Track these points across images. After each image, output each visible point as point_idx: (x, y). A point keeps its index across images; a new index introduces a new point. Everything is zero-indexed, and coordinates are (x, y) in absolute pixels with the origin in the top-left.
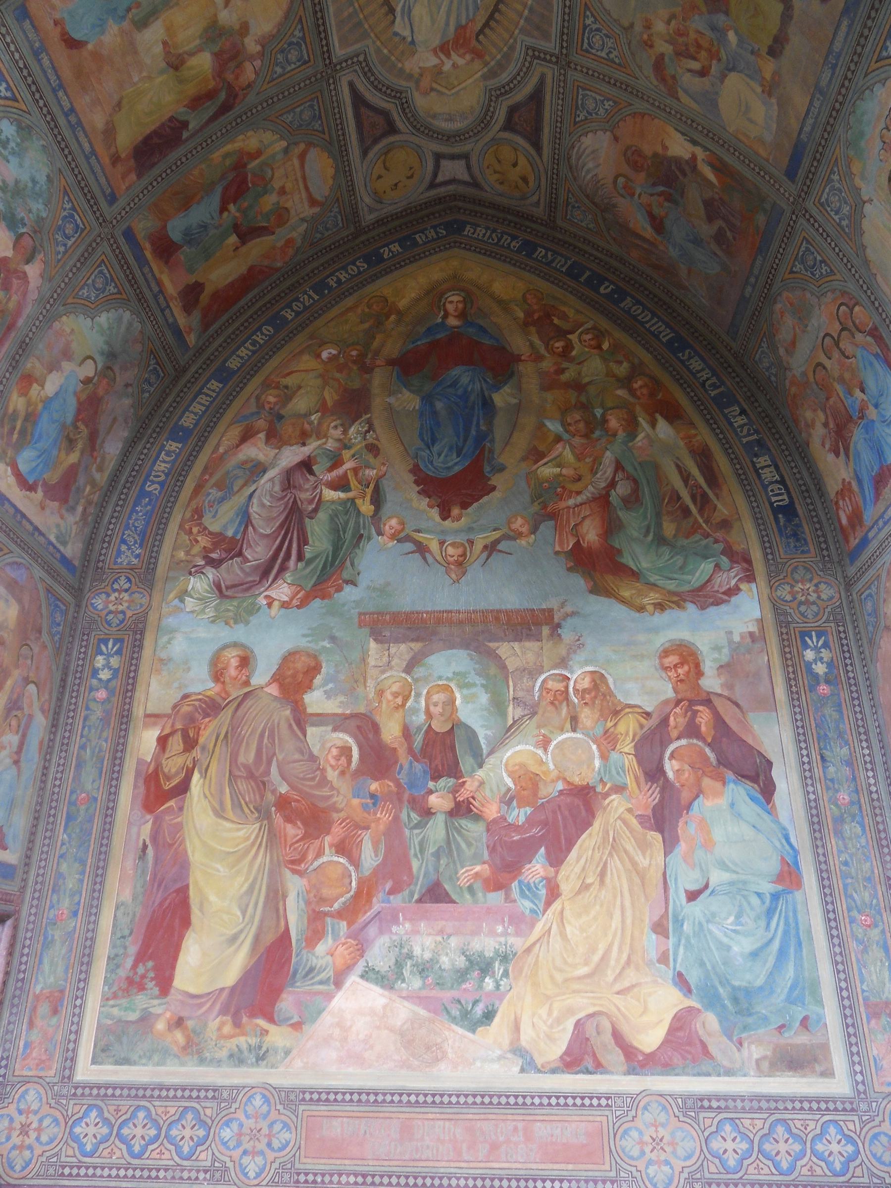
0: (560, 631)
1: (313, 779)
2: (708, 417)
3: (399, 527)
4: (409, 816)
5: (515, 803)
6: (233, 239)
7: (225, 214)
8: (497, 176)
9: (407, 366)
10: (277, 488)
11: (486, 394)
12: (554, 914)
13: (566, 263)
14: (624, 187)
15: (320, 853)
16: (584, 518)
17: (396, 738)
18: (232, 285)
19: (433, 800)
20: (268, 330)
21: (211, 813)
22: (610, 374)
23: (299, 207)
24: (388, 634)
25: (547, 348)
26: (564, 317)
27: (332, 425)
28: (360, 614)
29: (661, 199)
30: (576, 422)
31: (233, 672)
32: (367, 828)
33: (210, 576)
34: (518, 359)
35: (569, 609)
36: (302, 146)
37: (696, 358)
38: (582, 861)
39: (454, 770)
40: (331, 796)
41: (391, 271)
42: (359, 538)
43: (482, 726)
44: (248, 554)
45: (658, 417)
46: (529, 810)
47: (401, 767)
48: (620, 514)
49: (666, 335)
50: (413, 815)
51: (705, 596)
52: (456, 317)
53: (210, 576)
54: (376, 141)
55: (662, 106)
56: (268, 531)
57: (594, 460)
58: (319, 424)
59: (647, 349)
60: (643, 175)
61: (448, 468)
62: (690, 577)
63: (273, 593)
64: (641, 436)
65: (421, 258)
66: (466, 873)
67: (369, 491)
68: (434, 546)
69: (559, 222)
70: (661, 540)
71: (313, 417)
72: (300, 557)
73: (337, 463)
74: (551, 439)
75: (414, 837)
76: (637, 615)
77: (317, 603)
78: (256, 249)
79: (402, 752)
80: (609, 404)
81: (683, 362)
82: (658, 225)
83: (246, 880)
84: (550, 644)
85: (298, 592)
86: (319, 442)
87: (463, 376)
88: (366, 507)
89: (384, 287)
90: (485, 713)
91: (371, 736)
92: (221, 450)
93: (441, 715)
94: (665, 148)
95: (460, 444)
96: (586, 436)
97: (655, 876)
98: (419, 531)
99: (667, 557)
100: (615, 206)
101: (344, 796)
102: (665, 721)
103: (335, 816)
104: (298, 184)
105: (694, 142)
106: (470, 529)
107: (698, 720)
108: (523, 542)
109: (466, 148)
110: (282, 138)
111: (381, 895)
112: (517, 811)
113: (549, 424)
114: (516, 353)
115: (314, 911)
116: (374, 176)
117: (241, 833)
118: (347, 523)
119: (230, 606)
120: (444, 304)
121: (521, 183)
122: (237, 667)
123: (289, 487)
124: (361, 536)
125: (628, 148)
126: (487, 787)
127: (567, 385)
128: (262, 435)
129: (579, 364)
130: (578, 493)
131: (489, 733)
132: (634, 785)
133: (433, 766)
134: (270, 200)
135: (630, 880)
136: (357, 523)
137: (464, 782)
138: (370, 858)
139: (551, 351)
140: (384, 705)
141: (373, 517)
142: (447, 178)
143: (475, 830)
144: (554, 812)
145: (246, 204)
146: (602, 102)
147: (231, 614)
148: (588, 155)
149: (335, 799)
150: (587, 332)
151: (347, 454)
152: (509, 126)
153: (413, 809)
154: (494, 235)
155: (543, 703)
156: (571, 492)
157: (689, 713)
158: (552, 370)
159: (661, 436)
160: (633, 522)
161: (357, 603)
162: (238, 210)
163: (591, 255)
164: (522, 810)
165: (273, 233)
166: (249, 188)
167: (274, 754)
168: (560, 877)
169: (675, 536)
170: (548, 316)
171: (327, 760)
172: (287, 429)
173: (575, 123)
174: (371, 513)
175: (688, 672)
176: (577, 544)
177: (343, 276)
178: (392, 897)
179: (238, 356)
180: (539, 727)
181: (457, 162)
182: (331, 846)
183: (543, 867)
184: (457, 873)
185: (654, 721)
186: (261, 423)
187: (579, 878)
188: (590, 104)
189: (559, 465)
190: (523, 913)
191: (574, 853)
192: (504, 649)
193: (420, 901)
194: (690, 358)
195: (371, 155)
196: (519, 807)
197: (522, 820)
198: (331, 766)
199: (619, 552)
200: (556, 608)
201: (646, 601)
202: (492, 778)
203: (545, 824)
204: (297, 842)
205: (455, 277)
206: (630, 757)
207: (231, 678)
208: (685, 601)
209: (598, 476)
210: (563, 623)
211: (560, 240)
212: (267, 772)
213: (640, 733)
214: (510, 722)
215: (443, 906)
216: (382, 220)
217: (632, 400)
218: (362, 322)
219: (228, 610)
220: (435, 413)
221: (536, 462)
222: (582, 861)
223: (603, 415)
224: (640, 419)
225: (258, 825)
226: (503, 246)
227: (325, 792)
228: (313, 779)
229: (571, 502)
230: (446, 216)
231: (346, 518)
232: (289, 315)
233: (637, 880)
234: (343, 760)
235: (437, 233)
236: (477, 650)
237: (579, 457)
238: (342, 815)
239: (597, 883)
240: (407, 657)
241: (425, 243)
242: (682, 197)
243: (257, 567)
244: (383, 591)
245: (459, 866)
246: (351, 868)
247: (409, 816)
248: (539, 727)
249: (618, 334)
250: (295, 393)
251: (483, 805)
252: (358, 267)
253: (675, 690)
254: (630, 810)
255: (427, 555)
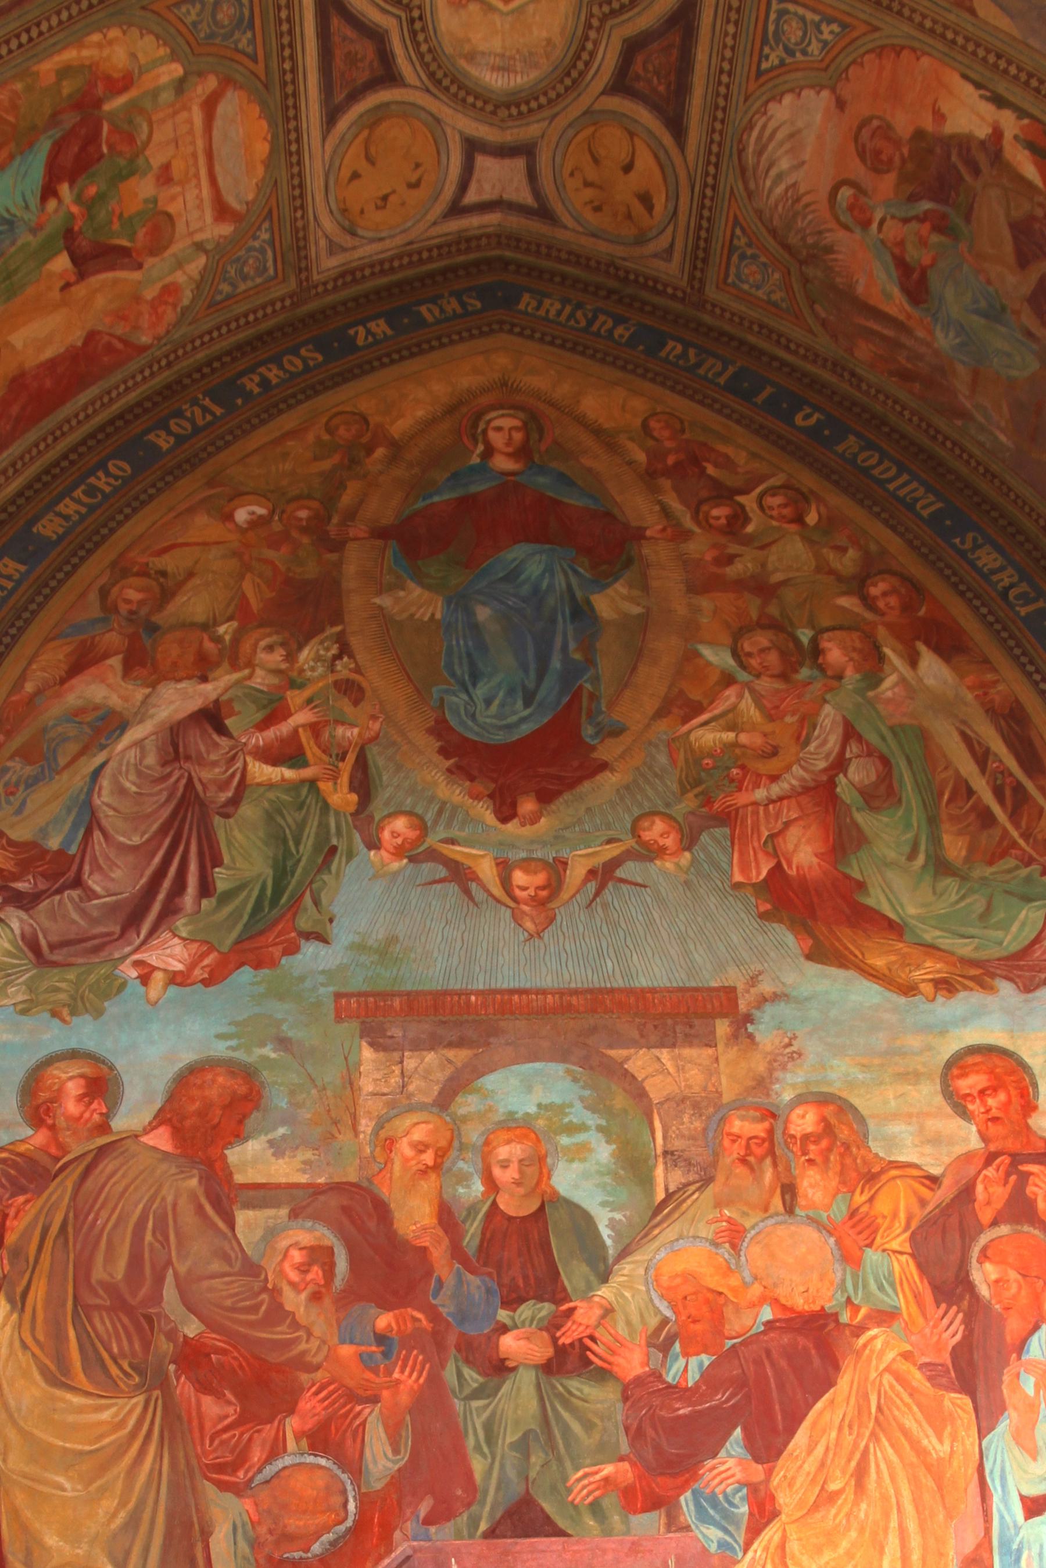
0: (750, 1028)
1: (254, 1309)
2: (1017, 651)
3: (412, 834)
4: (460, 1375)
5: (677, 1346)
6: (62, 263)
7: (52, 204)
8: (589, 193)
9: (416, 541)
10: (151, 760)
11: (579, 594)
12: (766, 1549)
13: (725, 369)
14: (851, 208)
15: (276, 1450)
16: (787, 825)
17: (425, 1229)
18: (51, 364)
19: (509, 1343)
20: (120, 467)
21: (37, 1377)
22: (823, 568)
23: (196, 220)
24: (397, 1032)
25: (695, 517)
26: (727, 464)
27: (263, 644)
28: (338, 996)
29: (926, 227)
30: (762, 651)
31: (72, 1107)
32: (375, 1400)
33: (15, 925)
34: (639, 535)
35: (766, 987)
36: (212, 83)
37: (987, 548)
38: (820, 1450)
39: (549, 1287)
40: (296, 1341)
41: (373, 369)
42: (328, 854)
43: (604, 1204)
44: (94, 883)
45: (922, 648)
46: (706, 1360)
47: (440, 1283)
48: (859, 817)
49: (928, 505)
50: (468, 1372)
51: (1031, 969)
52: (509, 455)
53: (15, 925)
54: (354, 97)
55: (939, 29)
56: (136, 840)
57: (802, 720)
58: (236, 641)
59: (893, 528)
60: (890, 179)
61: (509, 727)
62: (1000, 934)
63: (152, 957)
64: (888, 683)
65: (432, 348)
66: (585, 1479)
67: (346, 767)
68: (487, 870)
69: (711, 292)
70: (941, 867)
71: (221, 630)
72: (206, 889)
73: (275, 714)
74: (714, 678)
75: (473, 1416)
76: (902, 1000)
77: (245, 975)
78: (104, 289)
79: (439, 1254)
80: (826, 623)
81: (962, 554)
82: (916, 285)
83: (122, 1504)
84: (733, 1053)
85: (203, 956)
86: (236, 676)
87: (532, 562)
88: (341, 796)
89: (359, 396)
90: (608, 1179)
91: (372, 1225)
92: (29, 687)
93: (518, 1183)
94: (939, 117)
95: (531, 685)
96: (784, 676)
97: (963, 1471)
98: (453, 841)
99: (954, 897)
100: (829, 250)
101: (325, 1338)
102: (967, 1192)
103: (304, 1377)
104: (196, 164)
105: (999, 101)
106: (558, 839)
107: (1030, 1189)
108: (668, 865)
109: (532, 130)
110: (174, 56)
111: (410, 1526)
112: (681, 1362)
113: (707, 653)
114: (634, 524)
115: (270, 1559)
116: (346, 173)
117: (105, 1416)
118: (301, 826)
119: (62, 981)
120: (485, 432)
121: (638, 208)
122: (80, 1098)
123: (177, 758)
124: (333, 850)
125: (863, 124)
126: (620, 1317)
127: (739, 585)
128: (115, 662)
129: (762, 548)
130: (774, 778)
131: (618, 1216)
132: (914, 1309)
133: (506, 1280)
134: (144, 188)
135: (915, 1482)
136: (323, 826)
137: (572, 1310)
138: (381, 1459)
139: (706, 524)
140: (397, 1167)
141: (355, 814)
142: (486, 197)
143: (600, 1398)
144: (758, 1362)
145: (92, 191)
146: (818, 27)
147: (62, 996)
148: (781, 144)
149: (303, 1346)
150: (773, 491)
151: (295, 698)
152: (622, 84)
153: (467, 1361)
154: (579, 314)
155: (727, 1160)
156: (759, 776)
157: (1013, 1178)
158: (708, 557)
159: (930, 682)
160: (887, 834)
161: (329, 975)
162: (79, 200)
163: (774, 358)
164: (694, 1361)
165: (140, 266)
166: (102, 156)
167: (169, 1263)
168: (775, 1481)
169: (967, 859)
170: (695, 461)
171: (281, 1273)
172: (169, 649)
173: (759, 74)
174: (352, 809)
175: (1009, 1102)
176: (777, 870)
177: (273, 374)
178: (433, 1529)
179: (59, 514)
180: (718, 1204)
181: (507, 162)
182: (298, 1438)
183: (740, 1462)
184: (565, 1479)
185: (944, 1193)
186: (113, 638)
187: (813, 1481)
188: (793, 32)
189: (731, 727)
190: (705, 1550)
191: (801, 1437)
192: (640, 1062)
193: (491, 1534)
194: (976, 546)
195: (343, 124)
196: (686, 1354)
197: (693, 1377)
198: (291, 1284)
199: (861, 886)
200: (740, 987)
201: (917, 975)
202: (625, 1303)
203: (740, 1384)
204: (226, 1429)
205: (504, 384)
206: (903, 1258)
207: (69, 1118)
208: (993, 975)
209: (812, 747)
210: (757, 1013)
211: (710, 329)
212: (156, 1297)
213: (919, 1215)
214: (661, 1195)
215: (542, 1542)
216: (352, 272)
217: (869, 616)
218: (316, 459)
219: (58, 990)
220: (475, 628)
221: (685, 720)
222: (820, 1450)
223: (814, 641)
224: (887, 651)
225: (140, 1399)
226: (598, 334)
227: (281, 1333)
228: (254, 1309)
229: (760, 794)
230: (476, 283)
231: (299, 816)
232: (164, 442)
233: (929, 1482)
234: (316, 1273)
235: (463, 304)
236: (585, 1063)
237: (772, 715)
238: (320, 1376)
239: (850, 1492)
240: (441, 1076)
241: (438, 322)
242: (968, 219)
243: (112, 909)
244: (385, 951)
245: (568, 1464)
246: (344, 1477)
247: (460, 1375)
248: (718, 1204)
249: (837, 500)
250: (180, 585)
251: (614, 1353)
252: (304, 360)
253: (984, 1137)
254: (906, 1356)
255: (473, 886)
